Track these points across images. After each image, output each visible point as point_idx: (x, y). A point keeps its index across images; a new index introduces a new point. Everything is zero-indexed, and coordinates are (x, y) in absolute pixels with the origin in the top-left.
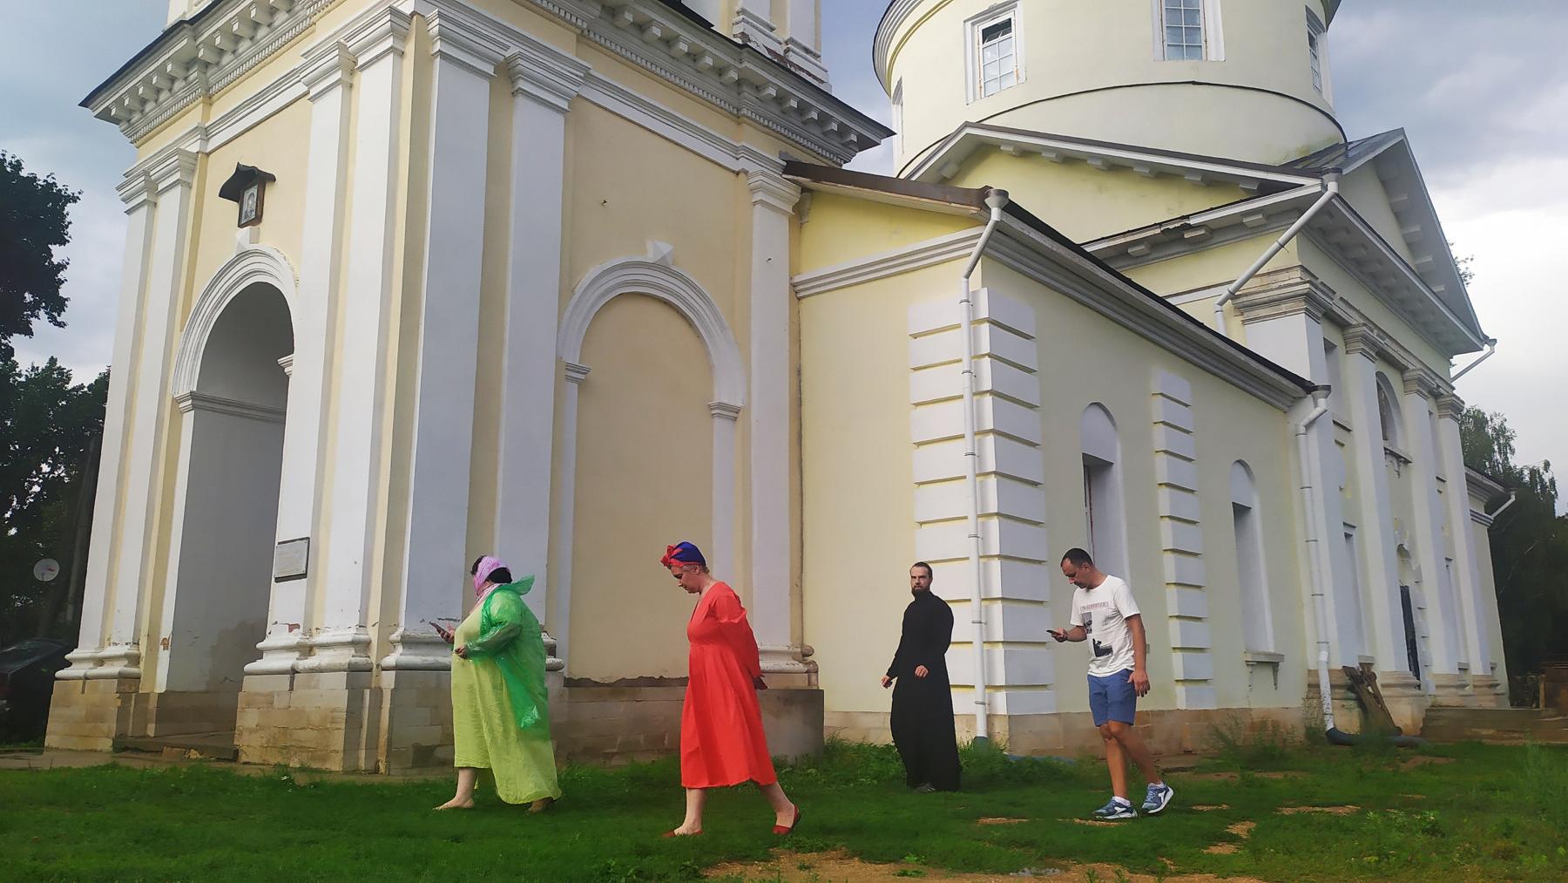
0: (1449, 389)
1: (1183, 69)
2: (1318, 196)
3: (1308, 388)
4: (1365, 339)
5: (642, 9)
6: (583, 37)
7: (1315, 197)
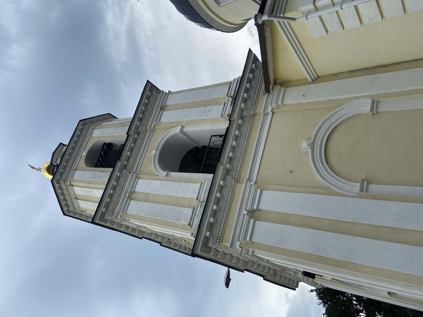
5: (225, 161)
6: (237, 181)
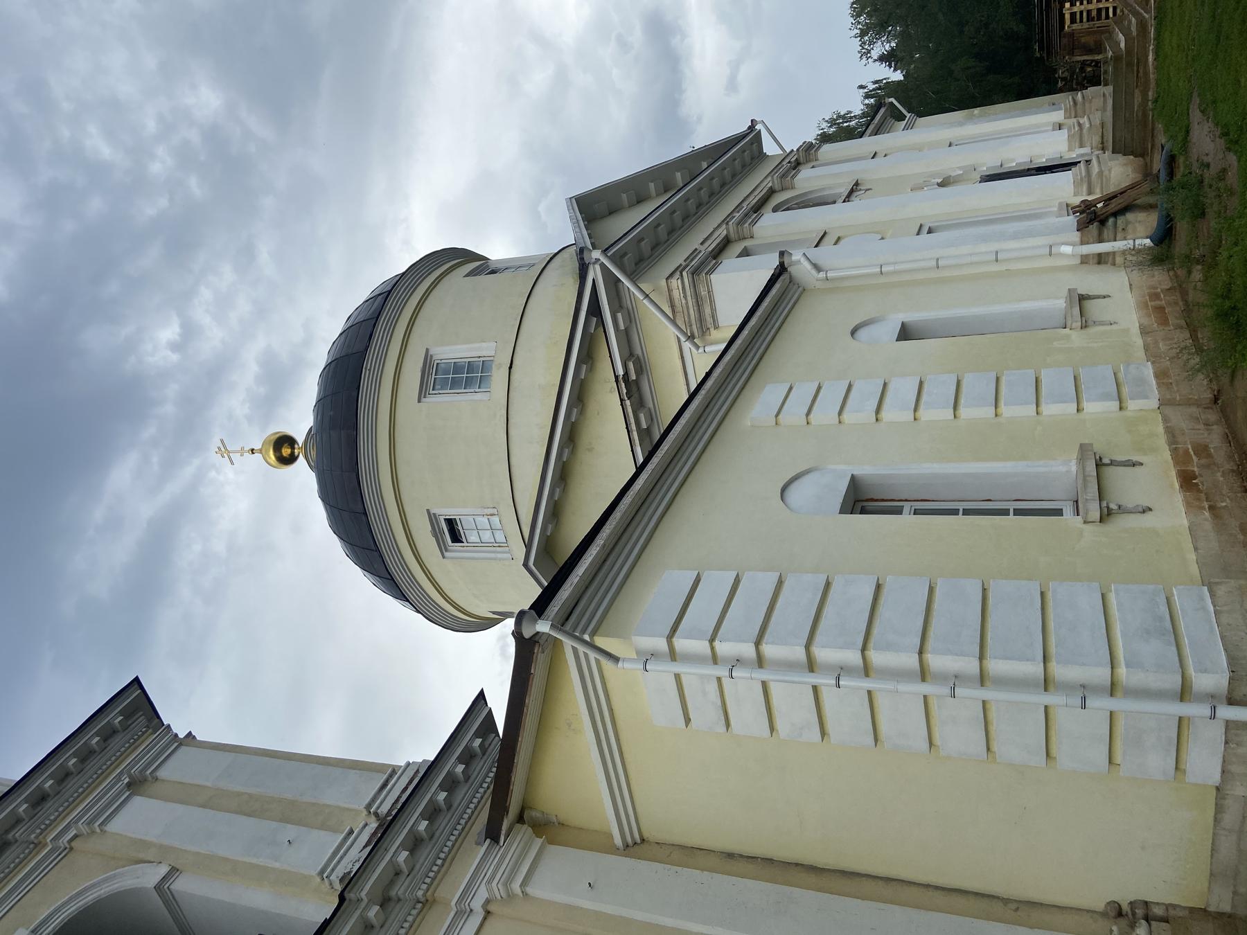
0: (793, 154)
1: (498, 377)
2: (603, 266)
3: (781, 270)
4: (741, 222)
7: (604, 269)
